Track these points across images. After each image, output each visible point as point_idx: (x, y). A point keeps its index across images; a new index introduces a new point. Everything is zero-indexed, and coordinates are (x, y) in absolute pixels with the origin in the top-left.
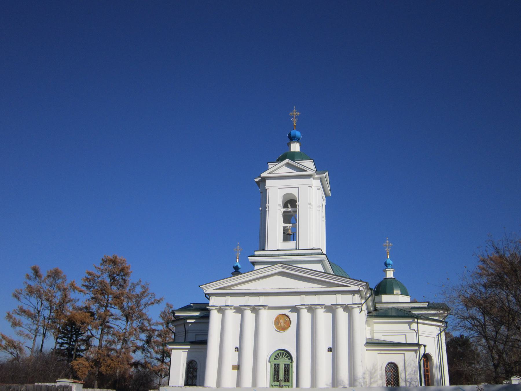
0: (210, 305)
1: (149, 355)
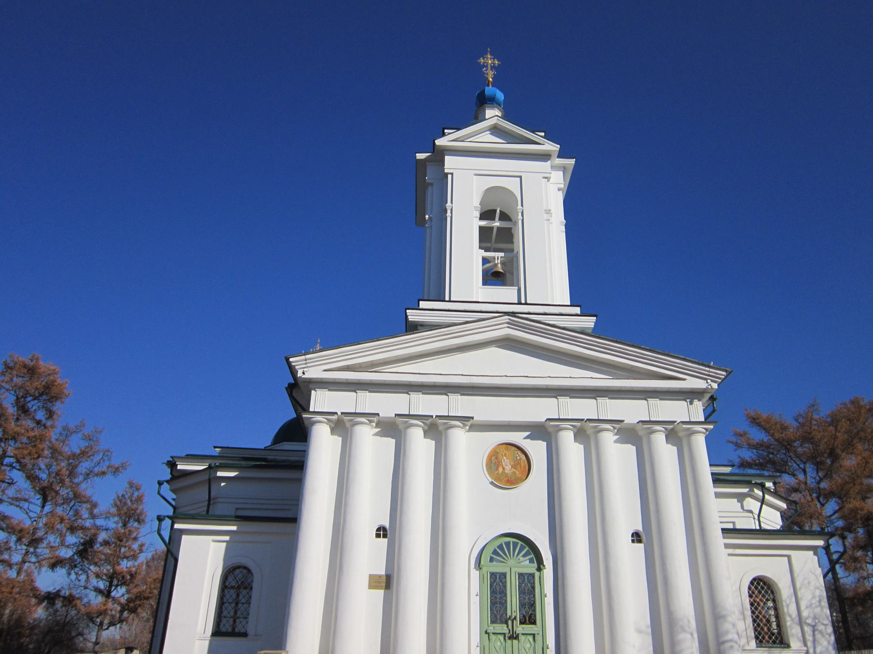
0: (311, 409)
1: (83, 577)
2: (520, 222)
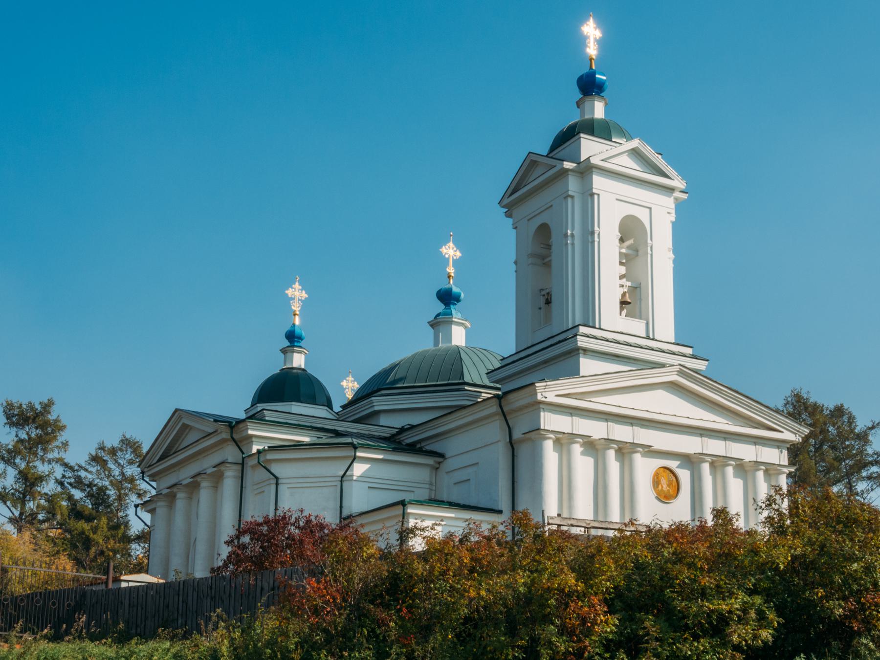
2: (649, 256)
